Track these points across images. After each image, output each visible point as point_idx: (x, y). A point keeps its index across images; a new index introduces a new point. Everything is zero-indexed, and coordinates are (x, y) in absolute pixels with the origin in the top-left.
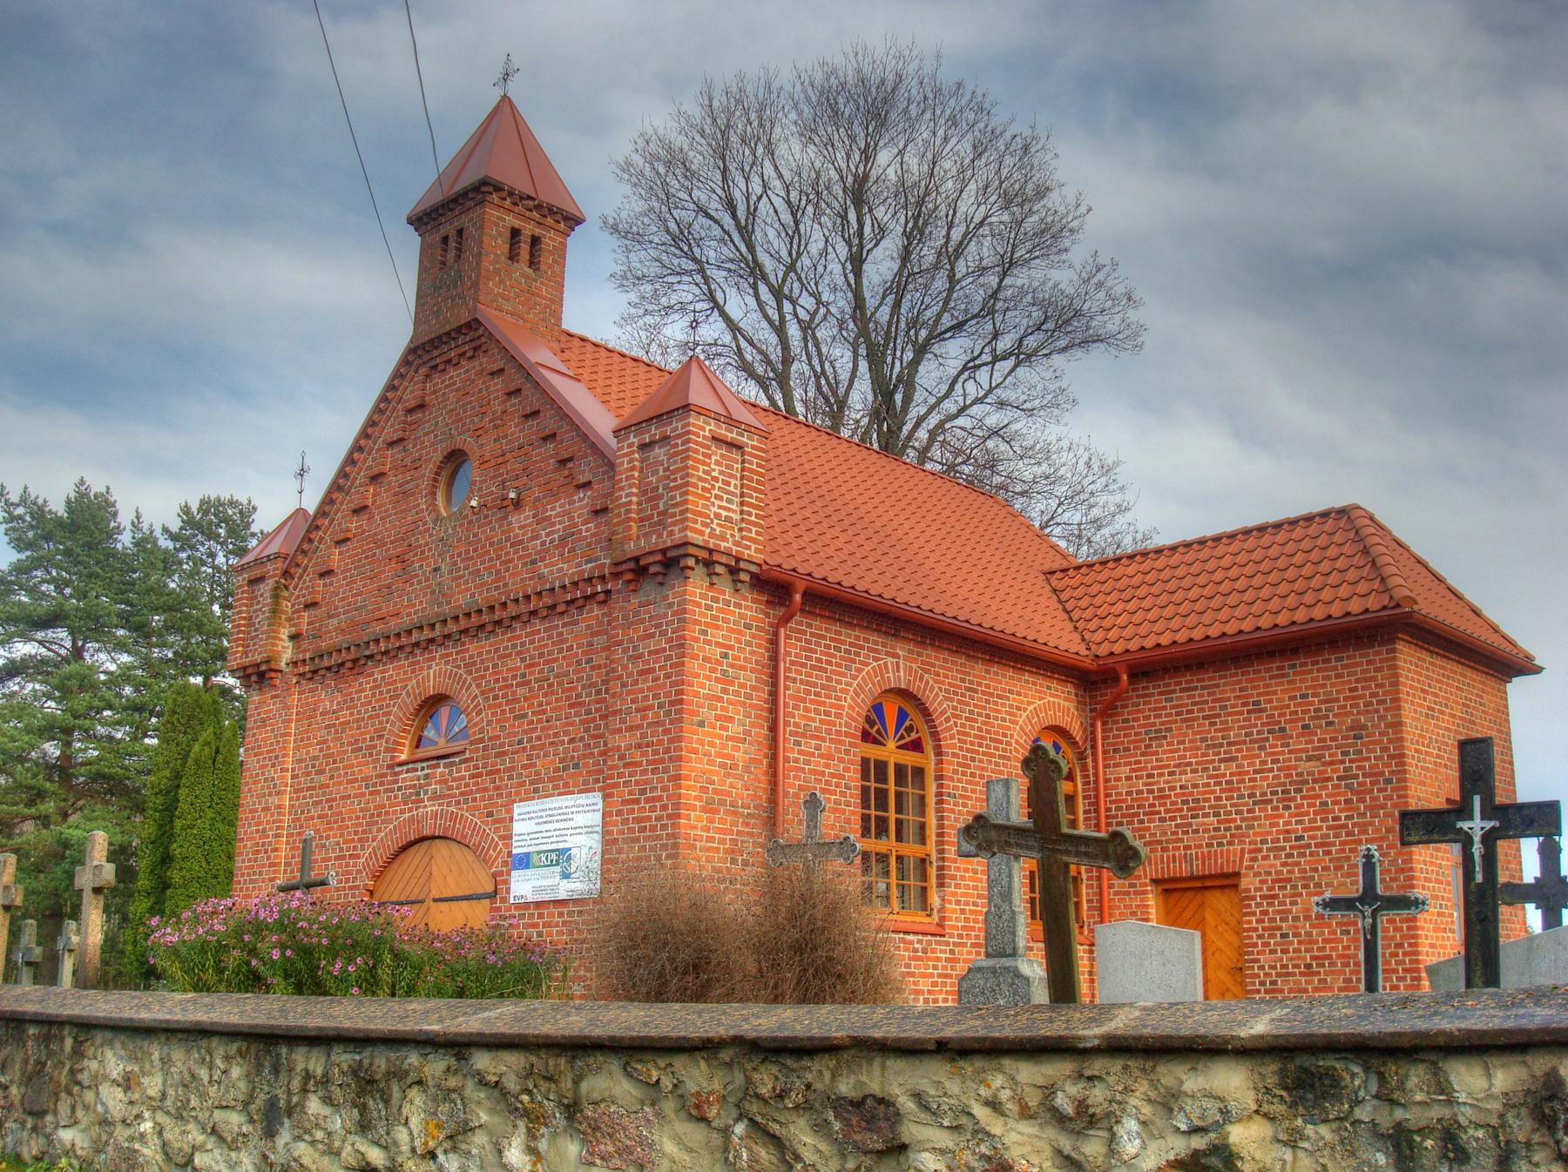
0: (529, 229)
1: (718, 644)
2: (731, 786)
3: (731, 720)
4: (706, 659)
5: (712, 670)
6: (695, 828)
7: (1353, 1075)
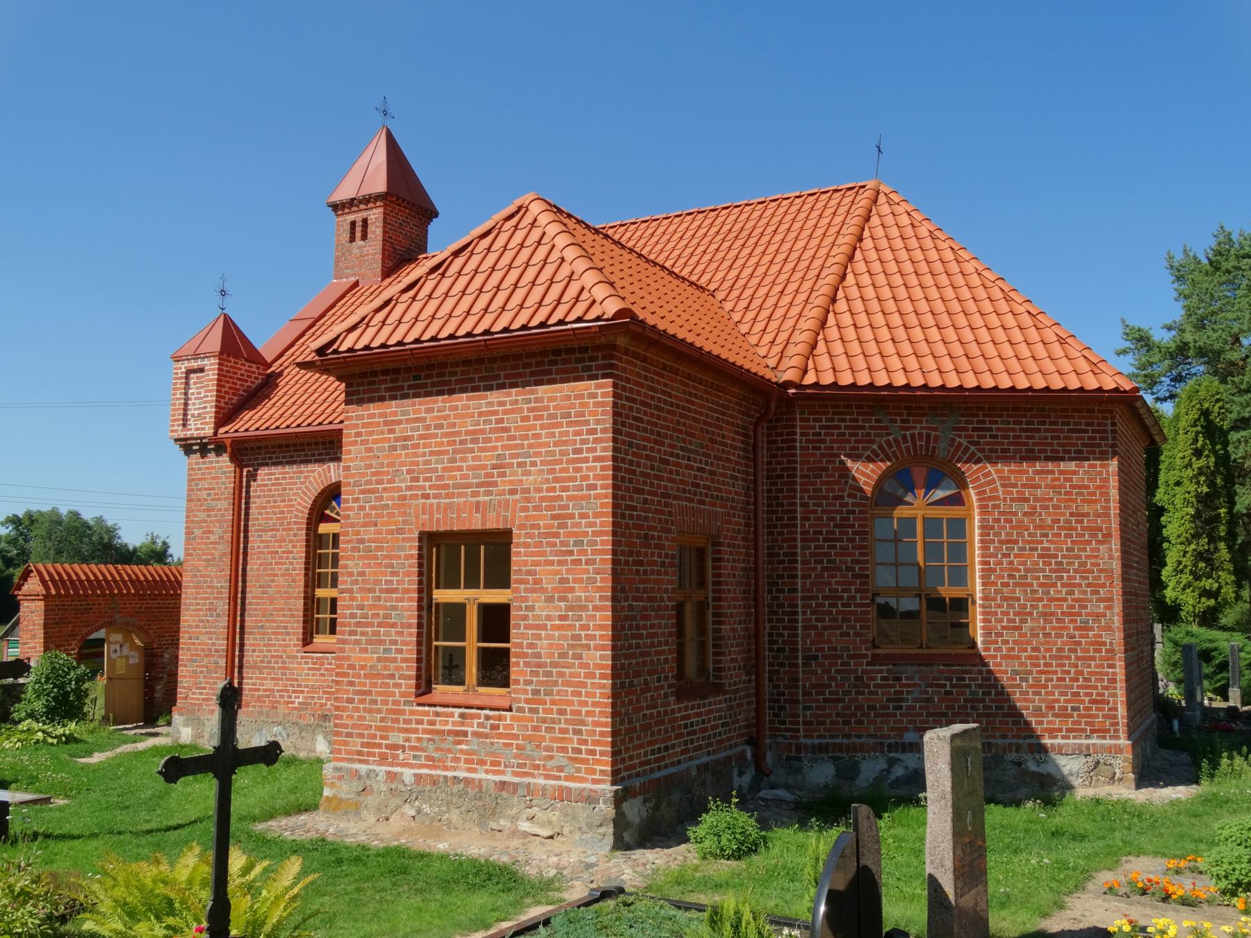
0: (358, 217)
4: (199, 500)
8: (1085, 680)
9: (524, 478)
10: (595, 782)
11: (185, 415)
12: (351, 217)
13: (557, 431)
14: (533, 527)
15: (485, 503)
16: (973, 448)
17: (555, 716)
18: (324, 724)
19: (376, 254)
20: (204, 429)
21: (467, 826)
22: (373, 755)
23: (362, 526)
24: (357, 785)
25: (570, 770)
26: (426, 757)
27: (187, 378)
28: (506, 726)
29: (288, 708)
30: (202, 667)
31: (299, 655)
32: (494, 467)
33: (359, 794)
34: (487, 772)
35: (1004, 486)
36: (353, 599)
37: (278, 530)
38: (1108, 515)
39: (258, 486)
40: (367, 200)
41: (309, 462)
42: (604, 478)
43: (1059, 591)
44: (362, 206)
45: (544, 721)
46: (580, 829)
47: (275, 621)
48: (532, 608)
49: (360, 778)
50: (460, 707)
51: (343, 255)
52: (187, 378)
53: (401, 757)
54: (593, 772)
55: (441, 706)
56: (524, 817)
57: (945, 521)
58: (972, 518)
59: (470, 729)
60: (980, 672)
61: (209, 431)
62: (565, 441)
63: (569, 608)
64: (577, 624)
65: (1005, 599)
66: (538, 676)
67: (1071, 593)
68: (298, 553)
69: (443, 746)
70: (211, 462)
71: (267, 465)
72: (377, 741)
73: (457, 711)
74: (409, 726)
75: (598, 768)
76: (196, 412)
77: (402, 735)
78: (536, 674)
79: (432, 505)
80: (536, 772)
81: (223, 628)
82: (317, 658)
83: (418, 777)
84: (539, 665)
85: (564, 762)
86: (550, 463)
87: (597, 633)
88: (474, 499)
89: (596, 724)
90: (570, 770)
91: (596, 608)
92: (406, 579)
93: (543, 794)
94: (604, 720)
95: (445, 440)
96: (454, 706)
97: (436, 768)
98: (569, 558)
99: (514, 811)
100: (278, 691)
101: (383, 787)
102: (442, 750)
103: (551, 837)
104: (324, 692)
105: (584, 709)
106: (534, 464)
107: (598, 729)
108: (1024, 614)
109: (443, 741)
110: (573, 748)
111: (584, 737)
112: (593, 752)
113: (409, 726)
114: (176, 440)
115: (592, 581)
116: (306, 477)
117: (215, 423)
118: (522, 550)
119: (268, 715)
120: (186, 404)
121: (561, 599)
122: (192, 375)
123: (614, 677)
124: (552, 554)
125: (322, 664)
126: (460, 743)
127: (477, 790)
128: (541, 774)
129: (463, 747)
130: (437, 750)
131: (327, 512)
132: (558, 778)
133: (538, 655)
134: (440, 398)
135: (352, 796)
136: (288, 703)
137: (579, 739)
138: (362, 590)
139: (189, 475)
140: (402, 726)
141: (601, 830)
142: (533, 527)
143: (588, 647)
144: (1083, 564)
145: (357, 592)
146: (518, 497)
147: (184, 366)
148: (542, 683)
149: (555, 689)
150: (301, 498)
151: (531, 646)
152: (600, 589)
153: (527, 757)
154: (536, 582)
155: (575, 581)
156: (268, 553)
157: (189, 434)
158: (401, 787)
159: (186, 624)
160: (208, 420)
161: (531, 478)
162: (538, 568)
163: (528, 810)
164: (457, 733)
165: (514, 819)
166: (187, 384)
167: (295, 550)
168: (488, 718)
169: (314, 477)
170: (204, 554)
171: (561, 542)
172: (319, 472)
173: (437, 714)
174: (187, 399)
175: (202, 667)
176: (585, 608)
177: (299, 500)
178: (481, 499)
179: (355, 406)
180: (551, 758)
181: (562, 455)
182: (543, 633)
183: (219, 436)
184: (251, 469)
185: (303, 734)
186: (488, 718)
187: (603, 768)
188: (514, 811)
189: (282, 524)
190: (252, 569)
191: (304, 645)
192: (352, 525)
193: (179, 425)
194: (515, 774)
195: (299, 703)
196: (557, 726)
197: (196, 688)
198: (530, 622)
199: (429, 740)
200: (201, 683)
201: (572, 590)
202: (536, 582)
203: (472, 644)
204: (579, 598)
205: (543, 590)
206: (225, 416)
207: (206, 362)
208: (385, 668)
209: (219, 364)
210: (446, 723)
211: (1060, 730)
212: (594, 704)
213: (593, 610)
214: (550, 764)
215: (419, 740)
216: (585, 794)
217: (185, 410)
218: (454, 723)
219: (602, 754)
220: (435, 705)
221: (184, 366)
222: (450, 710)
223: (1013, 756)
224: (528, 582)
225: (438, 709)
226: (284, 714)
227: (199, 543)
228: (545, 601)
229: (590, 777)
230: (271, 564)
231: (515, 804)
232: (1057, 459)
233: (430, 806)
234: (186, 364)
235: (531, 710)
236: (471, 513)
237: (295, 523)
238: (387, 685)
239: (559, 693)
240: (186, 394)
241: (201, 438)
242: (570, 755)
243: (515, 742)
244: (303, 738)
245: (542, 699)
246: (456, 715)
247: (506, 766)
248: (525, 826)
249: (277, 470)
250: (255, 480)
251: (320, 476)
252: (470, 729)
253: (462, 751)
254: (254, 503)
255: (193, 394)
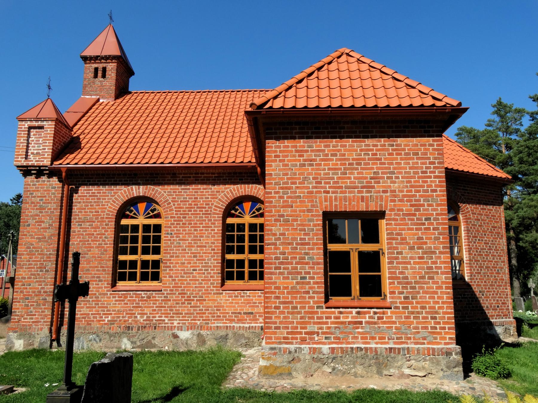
0: (100, 66)
1: (38, 197)
2: (42, 245)
3: (43, 222)
4: (32, 203)
5: (36, 206)
6: (24, 261)
7: (145, 381)
8: (500, 294)
9: (392, 185)
10: (446, 344)
11: (27, 152)
12: (96, 65)
13: (411, 161)
14: (398, 210)
15: (367, 197)
16: (462, 197)
17: (419, 310)
18: (128, 332)
19: (111, 86)
20: (43, 161)
21: (369, 375)
22: (296, 338)
23: (282, 208)
24: (287, 357)
25: (430, 338)
26: (334, 337)
27: (29, 131)
28: (388, 317)
29: (100, 324)
30: (33, 302)
31: (109, 293)
32: (372, 178)
33: (290, 362)
34: (377, 343)
35: (472, 214)
36: (276, 249)
37: (94, 222)
38: (501, 228)
39: (79, 196)
40: (107, 58)
41: (118, 184)
42: (441, 186)
43: (490, 258)
44: (103, 61)
45: (413, 313)
46: (442, 370)
47: (91, 274)
48: (401, 253)
49: (290, 352)
50: (356, 308)
51: (89, 84)
52: (29, 131)
53: (316, 339)
54: (445, 338)
55: (343, 308)
56: (405, 366)
57: (453, 228)
58: (460, 225)
59: (364, 320)
60: (470, 292)
61: (47, 162)
62: (416, 167)
63: (425, 253)
64: (430, 261)
65: (476, 261)
66: (407, 289)
67: (494, 259)
68: (108, 234)
69: (345, 330)
70: (44, 181)
71: (86, 185)
72: (299, 330)
73: (354, 311)
74: (321, 320)
75: (448, 336)
76: (35, 152)
77: (316, 326)
78: (406, 288)
79: (331, 197)
80: (409, 341)
81: (51, 278)
82: (122, 294)
83: (333, 349)
84: (407, 283)
85: (426, 334)
86: (407, 177)
87: (443, 266)
88: (360, 195)
89: (444, 313)
90: (430, 338)
91: (440, 253)
92: (315, 238)
93: (417, 353)
94: (449, 311)
95: (339, 162)
96: (335, 308)
97: (342, 343)
98: (423, 227)
99: (400, 363)
100: (92, 314)
101: (308, 357)
102: (345, 333)
103: (425, 376)
104: (127, 314)
105: (437, 306)
106: (397, 178)
107: (446, 316)
108: (481, 267)
109: (346, 328)
110: (431, 327)
111: (438, 320)
112: (444, 328)
113: (321, 320)
114: (18, 167)
115: (437, 239)
116: (115, 193)
117: (52, 158)
118: (393, 222)
119: (85, 329)
120: (28, 146)
121: (419, 248)
122: (32, 130)
123: (454, 289)
124: (412, 224)
125: (126, 297)
126: (358, 328)
127: (374, 353)
128: (412, 342)
129: (360, 330)
130: (341, 333)
131: (128, 213)
132: (424, 344)
133: (407, 278)
134: (334, 140)
135: (285, 364)
136: (100, 321)
137: (434, 322)
138: (283, 244)
139: (25, 188)
140: (316, 320)
141: (456, 369)
142: (398, 210)
143: (437, 273)
144: (496, 247)
145: (280, 245)
146: (388, 194)
147: (27, 125)
148: (410, 293)
149: (418, 296)
150: (111, 204)
151: (401, 273)
152: (442, 243)
153: (403, 333)
154: (402, 239)
155: (426, 238)
156: (86, 235)
157: (30, 163)
158: (321, 356)
159: (20, 277)
160: (46, 156)
161: (396, 185)
162: (403, 232)
163: (408, 362)
164: (355, 323)
165: (400, 367)
166: (29, 135)
167: (106, 233)
168: (375, 313)
169: (121, 193)
170: (35, 235)
171: (417, 218)
172: (125, 191)
173: (341, 313)
174: (28, 143)
175: (33, 302)
176: (434, 253)
177: (109, 205)
178: (364, 195)
179: (274, 141)
180: (418, 333)
181: (415, 174)
182: (409, 266)
183: (53, 166)
184: (74, 187)
185: (112, 338)
186: (375, 313)
187: (451, 336)
188: (400, 363)
189: (97, 219)
190: (73, 244)
191: (112, 288)
192: (275, 207)
193: (22, 158)
194: (395, 343)
195: (108, 321)
196: (420, 316)
197: (27, 315)
198: (400, 260)
199: (336, 328)
200: (31, 312)
201: (426, 243)
202: (402, 239)
203: (355, 274)
204: (430, 248)
205: (408, 244)
206: (57, 155)
207: (45, 123)
208: (302, 288)
209: (55, 125)
210: (347, 317)
211: (494, 316)
212: (443, 303)
213: (439, 254)
214: (418, 336)
215: (329, 328)
216: (444, 351)
217: (27, 149)
218: (352, 317)
219: (449, 328)
220: (339, 308)
221: (27, 125)
222: (350, 310)
223: (483, 327)
224: (397, 239)
225: (341, 310)
226: (98, 327)
227: (32, 228)
228: (409, 249)
229: (443, 342)
230: (88, 241)
231: (400, 360)
232: (487, 204)
233: (342, 366)
234: (29, 123)
235: (403, 308)
236: (358, 202)
237: (107, 218)
238: (305, 298)
239: (421, 298)
240: (28, 140)
241: (40, 167)
242: (430, 330)
243: (394, 326)
244: (112, 341)
245: (411, 302)
246: (354, 313)
247: (389, 339)
248: (407, 371)
249: (94, 189)
250: (77, 193)
251: (125, 193)
252: (364, 320)
253: (359, 333)
254: (76, 206)
255: (33, 141)
